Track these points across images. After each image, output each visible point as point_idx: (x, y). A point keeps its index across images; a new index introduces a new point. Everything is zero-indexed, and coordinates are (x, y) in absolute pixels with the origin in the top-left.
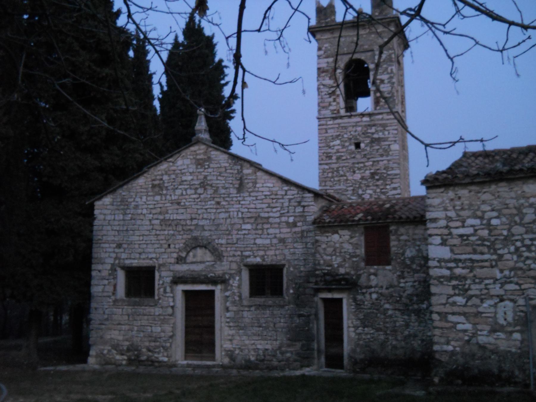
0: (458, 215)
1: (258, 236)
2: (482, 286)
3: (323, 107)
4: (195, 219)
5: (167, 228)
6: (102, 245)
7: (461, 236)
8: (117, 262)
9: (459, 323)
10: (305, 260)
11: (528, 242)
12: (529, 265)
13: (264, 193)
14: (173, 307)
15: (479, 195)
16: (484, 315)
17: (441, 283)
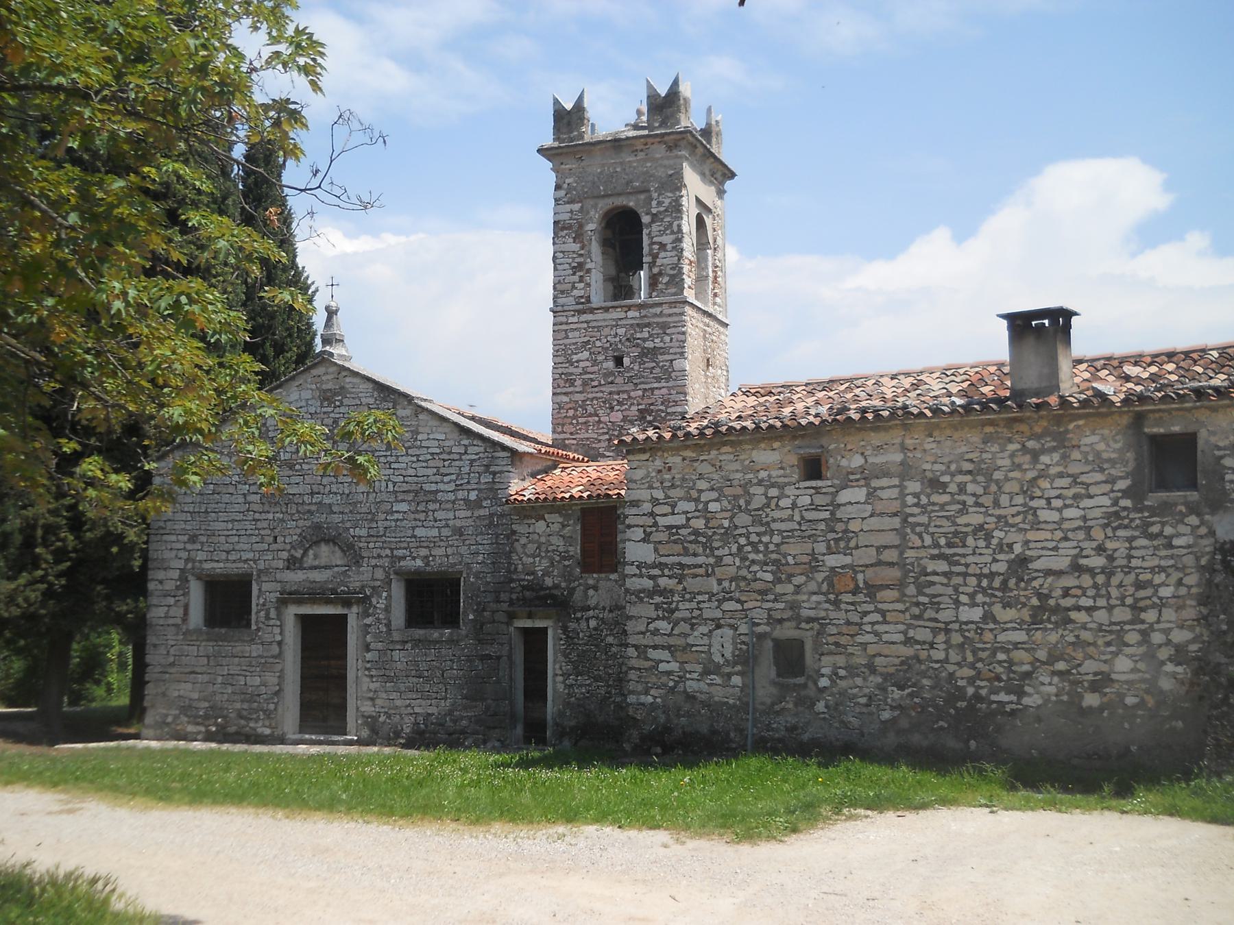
0: (667, 497)
1: (420, 524)
2: (694, 605)
3: (562, 292)
4: (318, 493)
5: (273, 510)
6: (165, 537)
7: (669, 527)
8: (190, 566)
9: (662, 661)
10: (493, 563)
11: (754, 538)
12: (755, 572)
13: (430, 450)
14: (280, 643)
15: (695, 464)
16: (694, 649)
17: (641, 600)
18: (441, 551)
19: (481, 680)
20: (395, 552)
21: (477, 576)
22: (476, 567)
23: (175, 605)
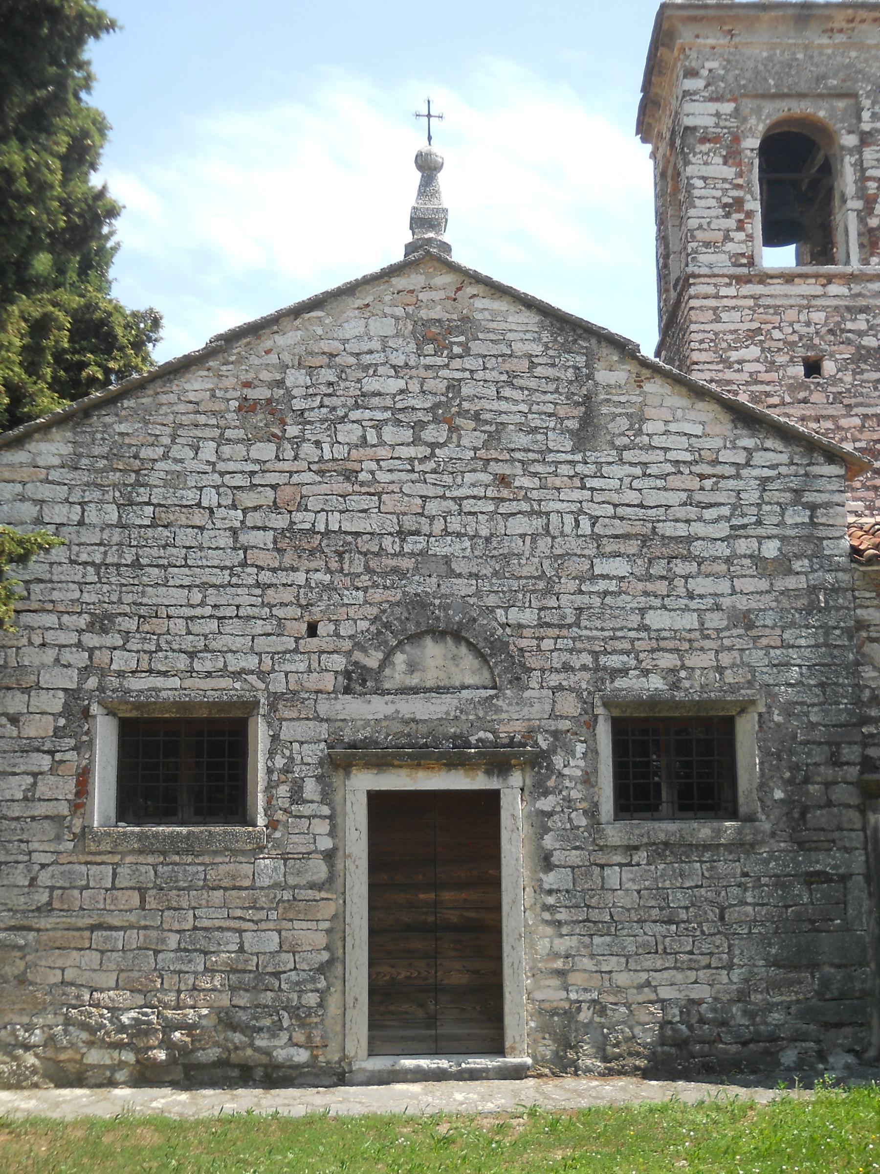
1: (657, 602)
4: (417, 533)
5: (305, 564)
8: (92, 683)
10: (822, 685)
13: (671, 456)
14: (329, 856)
18: (705, 660)
19: (806, 926)
20: (603, 660)
21: (788, 709)
22: (785, 694)
23: (53, 771)
